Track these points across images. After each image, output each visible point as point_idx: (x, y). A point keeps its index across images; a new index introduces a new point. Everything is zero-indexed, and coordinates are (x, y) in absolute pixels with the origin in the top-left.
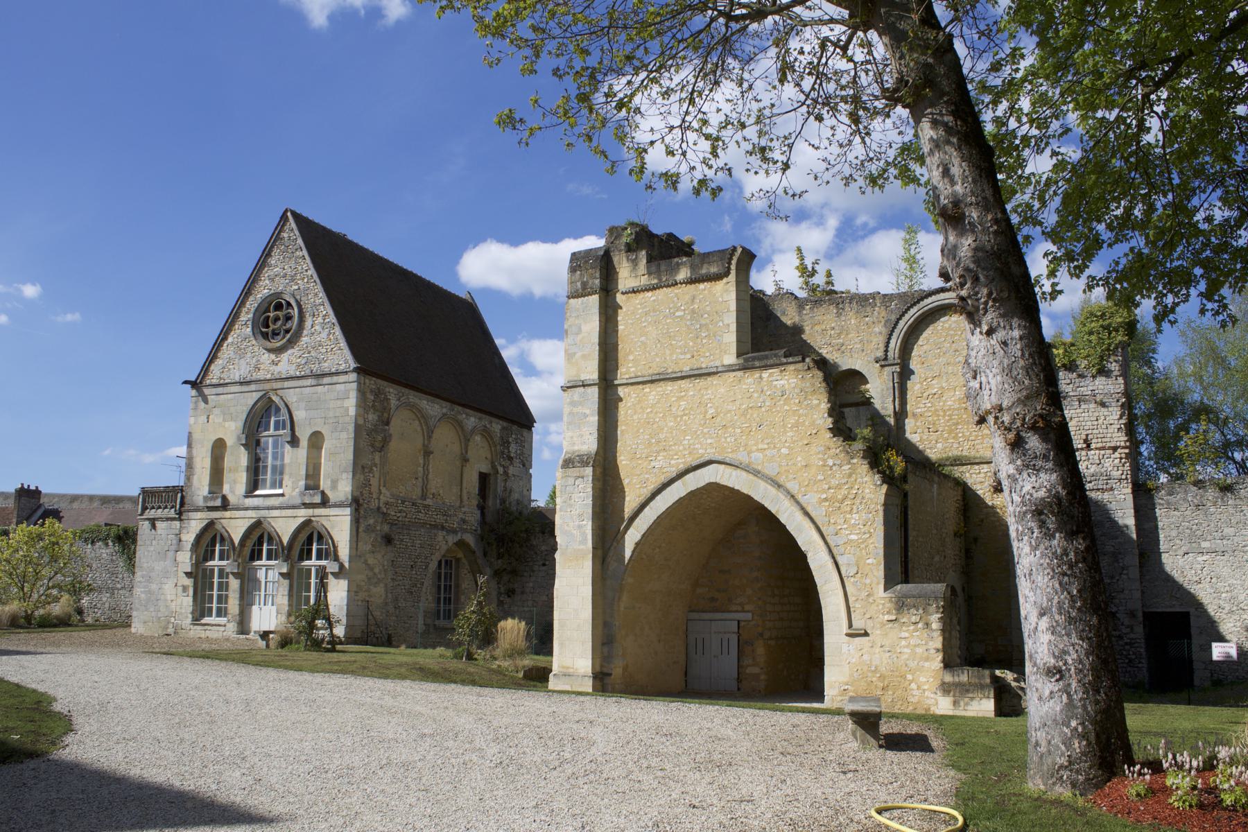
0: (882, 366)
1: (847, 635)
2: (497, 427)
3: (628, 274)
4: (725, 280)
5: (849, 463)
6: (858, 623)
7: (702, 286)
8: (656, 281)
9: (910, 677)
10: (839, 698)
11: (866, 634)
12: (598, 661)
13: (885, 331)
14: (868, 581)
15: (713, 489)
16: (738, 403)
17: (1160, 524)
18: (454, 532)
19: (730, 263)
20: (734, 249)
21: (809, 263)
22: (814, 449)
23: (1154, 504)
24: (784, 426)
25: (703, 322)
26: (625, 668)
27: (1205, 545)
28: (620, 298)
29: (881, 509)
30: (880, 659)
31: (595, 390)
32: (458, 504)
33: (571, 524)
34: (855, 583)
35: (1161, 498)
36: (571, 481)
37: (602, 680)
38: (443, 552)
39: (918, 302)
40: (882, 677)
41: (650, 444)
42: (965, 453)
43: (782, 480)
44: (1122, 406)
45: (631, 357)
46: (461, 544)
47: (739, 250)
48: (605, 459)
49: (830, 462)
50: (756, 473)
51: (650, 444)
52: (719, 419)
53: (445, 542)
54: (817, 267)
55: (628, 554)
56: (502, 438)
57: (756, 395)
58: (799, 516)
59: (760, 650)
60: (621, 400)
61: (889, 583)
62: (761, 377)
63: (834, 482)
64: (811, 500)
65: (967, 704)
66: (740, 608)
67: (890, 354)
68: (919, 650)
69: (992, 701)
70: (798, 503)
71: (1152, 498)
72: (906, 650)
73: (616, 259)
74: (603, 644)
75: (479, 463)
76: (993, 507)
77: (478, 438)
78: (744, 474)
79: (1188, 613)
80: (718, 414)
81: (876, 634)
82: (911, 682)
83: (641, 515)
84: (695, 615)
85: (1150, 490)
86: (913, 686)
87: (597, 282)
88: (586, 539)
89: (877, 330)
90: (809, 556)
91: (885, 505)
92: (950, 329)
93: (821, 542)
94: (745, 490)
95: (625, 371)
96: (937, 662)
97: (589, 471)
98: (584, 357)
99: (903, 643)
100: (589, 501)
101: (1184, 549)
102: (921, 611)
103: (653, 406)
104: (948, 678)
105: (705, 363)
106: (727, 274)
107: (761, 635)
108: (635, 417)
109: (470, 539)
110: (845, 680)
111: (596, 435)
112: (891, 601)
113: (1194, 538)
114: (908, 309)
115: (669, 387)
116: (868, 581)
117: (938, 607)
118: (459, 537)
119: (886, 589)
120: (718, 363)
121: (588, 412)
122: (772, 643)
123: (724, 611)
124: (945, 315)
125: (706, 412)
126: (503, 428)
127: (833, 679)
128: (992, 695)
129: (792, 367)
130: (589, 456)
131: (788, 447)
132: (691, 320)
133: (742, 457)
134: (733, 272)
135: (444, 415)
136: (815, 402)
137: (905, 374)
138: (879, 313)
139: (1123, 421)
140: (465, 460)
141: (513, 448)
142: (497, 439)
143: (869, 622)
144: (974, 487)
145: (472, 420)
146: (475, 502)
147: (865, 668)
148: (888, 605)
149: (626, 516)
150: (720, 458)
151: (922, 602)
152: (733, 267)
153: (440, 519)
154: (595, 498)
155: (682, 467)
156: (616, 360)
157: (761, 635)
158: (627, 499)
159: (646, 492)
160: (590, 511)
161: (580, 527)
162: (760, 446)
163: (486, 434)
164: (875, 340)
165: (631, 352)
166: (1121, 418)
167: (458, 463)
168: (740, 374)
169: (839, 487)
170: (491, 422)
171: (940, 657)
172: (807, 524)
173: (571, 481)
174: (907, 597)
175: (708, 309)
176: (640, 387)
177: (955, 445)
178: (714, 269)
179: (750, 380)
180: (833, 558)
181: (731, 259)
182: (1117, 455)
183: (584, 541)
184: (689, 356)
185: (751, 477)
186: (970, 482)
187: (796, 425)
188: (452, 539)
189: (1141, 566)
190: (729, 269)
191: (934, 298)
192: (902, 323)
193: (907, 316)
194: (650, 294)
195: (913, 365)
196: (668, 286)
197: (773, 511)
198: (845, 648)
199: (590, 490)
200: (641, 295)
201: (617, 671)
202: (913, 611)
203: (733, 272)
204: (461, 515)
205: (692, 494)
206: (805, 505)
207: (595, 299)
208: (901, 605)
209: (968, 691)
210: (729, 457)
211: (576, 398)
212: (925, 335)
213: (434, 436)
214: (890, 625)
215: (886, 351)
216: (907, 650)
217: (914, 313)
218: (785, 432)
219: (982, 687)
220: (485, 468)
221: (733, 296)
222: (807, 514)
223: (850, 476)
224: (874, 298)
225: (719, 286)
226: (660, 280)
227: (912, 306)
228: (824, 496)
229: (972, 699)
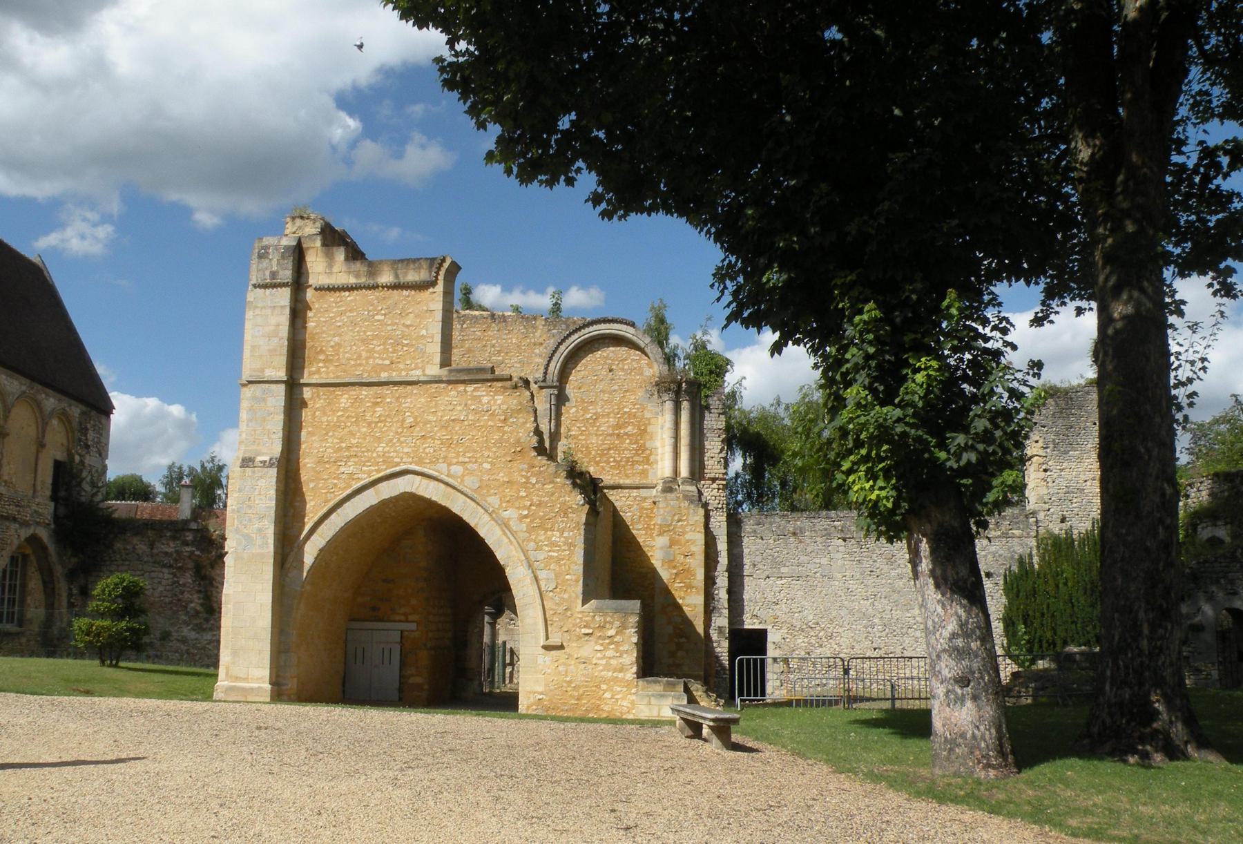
2: (76, 411)
4: (431, 290)
9: (604, 687)
11: (561, 647)
15: (410, 501)
18: (25, 524)
19: (437, 273)
20: (444, 260)
27: (784, 570)
30: (578, 673)
31: (282, 387)
32: (30, 493)
35: (748, 526)
38: (14, 547)
46: (34, 540)
52: (418, 429)
53: (16, 536)
56: (80, 423)
57: (459, 408)
61: (587, 597)
66: (403, 618)
67: (549, 377)
75: (55, 450)
77: (55, 422)
78: (443, 486)
79: (765, 631)
82: (605, 691)
86: (608, 695)
92: (606, 358)
99: (599, 655)
101: (767, 573)
103: (345, 410)
106: (433, 284)
109: (44, 534)
113: (776, 564)
118: (30, 531)
119: (585, 602)
123: (411, 619)
125: (404, 420)
126: (83, 413)
131: (491, 463)
135: (24, 392)
137: (561, 399)
140: (41, 445)
141: (91, 435)
142: (75, 424)
145: (51, 402)
146: (48, 493)
152: (441, 277)
153: (13, 510)
160: (273, 515)
162: (461, 459)
163: (64, 417)
167: (34, 448)
170: (70, 405)
178: (412, 276)
181: (439, 269)
182: (715, 486)
187: (500, 441)
188: (25, 533)
190: (436, 277)
192: (562, 348)
194: (347, 293)
195: (570, 390)
197: (472, 525)
198: (540, 660)
204: (34, 507)
205: (384, 503)
213: (13, 414)
215: (545, 373)
217: (576, 339)
220: (61, 456)
228: (526, 512)
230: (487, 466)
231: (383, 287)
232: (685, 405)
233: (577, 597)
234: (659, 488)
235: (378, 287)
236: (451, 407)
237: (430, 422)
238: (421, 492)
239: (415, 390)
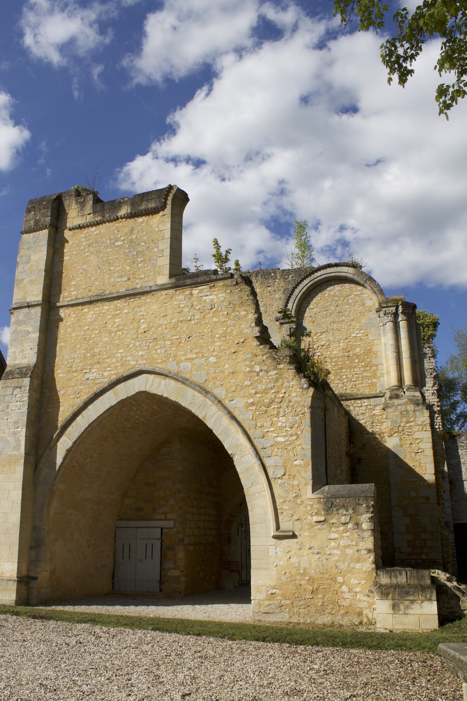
0: (281, 324)
1: (275, 537)
3: (74, 215)
4: (161, 213)
5: (276, 369)
6: (285, 525)
7: (140, 220)
8: (100, 218)
9: (340, 579)
10: (267, 603)
11: (294, 536)
12: (25, 565)
13: (284, 297)
14: (295, 482)
15: (144, 397)
16: (168, 317)
17: (462, 460)
19: (166, 199)
21: (223, 251)
22: (241, 356)
23: (457, 447)
24: (213, 337)
25: (140, 249)
26: (53, 572)
28: (67, 234)
29: (307, 411)
30: (309, 561)
31: (38, 310)
33: (7, 431)
34: (282, 485)
36: (9, 391)
37: (27, 584)
39: (310, 275)
40: (311, 580)
41: (85, 357)
42: (348, 391)
43: (209, 387)
44: (434, 377)
45: (73, 283)
47: (175, 190)
48: (43, 373)
49: (257, 368)
50: (184, 381)
51: (85, 357)
52: (151, 333)
54: (229, 257)
55: (59, 460)
57: (186, 310)
58: (226, 420)
59: (181, 555)
60: (61, 320)
61: (318, 482)
62: (191, 294)
63: (261, 387)
64: (238, 405)
65: (407, 607)
66: (163, 517)
68: (349, 551)
69: (435, 603)
70: (225, 407)
71: (455, 442)
72: (336, 552)
73: (66, 203)
74: (31, 548)
76: (373, 434)
78: (173, 382)
80: (150, 328)
81: (304, 535)
82: (342, 584)
83: (74, 424)
84: (123, 523)
85: (455, 436)
86: (344, 588)
87: (48, 219)
88: (19, 445)
89: (277, 296)
90: (235, 459)
91: (312, 407)
92: (334, 296)
93: (248, 445)
94: (173, 398)
95: (65, 297)
96: (368, 563)
97: (27, 381)
98: (31, 282)
99: (333, 544)
100: (25, 409)
102: (351, 511)
104: (385, 580)
105: (139, 285)
106: (163, 208)
107: (182, 541)
108: (73, 335)
110: (273, 583)
111: (36, 350)
112: (319, 502)
114: (302, 280)
115: (106, 306)
116: (295, 482)
117: (368, 507)
119: (314, 491)
120: (151, 284)
121: (30, 329)
122: (191, 548)
124: (331, 285)
125: (139, 327)
127: (260, 583)
128: (434, 597)
129: (221, 283)
130: (27, 368)
131: (216, 356)
132: (129, 248)
133: (171, 367)
134: (169, 207)
136: (243, 313)
138: (279, 283)
139: (436, 388)
143: (297, 523)
144: (357, 418)
147: (294, 571)
148: (317, 506)
149: (59, 425)
150: (150, 368)
151: (352, 503)
152: (169, 202)
154: (30, 407)
155: (114, 378)
156: (60, 286)
157: (182, 541)
158: (61, 409)
159: (79, 402)
160: (25, 418)
161: (14, 433)
162: (189, 356)
164: (276, 304)
165: (73, 278)
166: (434, 386)
168: (171, 292)
169: (265, 392)
171: (372, 558)
172: (234, 428)
173: (9, 391)
174: (336, 497)
175: (145, 238)
176: (80, 308)
177: (340, 385)
178: (152, 205)
179: (181, 297)
180: (260, 460)
183: (17, 447)
184: (125, 279)
185: (179, 385)
186: (353, 414)
187: (224, 335)
189: (451, 490)
191: (322, 272)
192: (297, 291)
193: (301, 286)
194: (94, 229)
196: (110, 221)
197: (201, 417)
198: (272, 551)
199: (26, 399)
200: (86, 231)
201: (43, 574)
202: (343, 511)
203: (169, 207)
205: (122, 403)
206: (231, 410)
207: (44, 233)
208: (330, 506)
209: (407, 593)
210: (159, 367)
211: (21, 317)
212: (315, 300)
214: (319, 526)
216: (337, 552)
218: (213, 342)
219: (423, 589)
221: (168, 226)
222: (233, 418)
223: (277, 380)
224: (275, 273)
225: (156, 219)
226: (104, 217)
227: (305, 278)
228: (251, 400)
229: (413, 602)
230: (212, 359)
231: (122, 218)
232: (403, 325)
233: (306, 484)
234: (388, 395)
235: (118, 219)
236: (179, 310)
237: (161, 325)
238: (154, 390)
239: (147, 299)
